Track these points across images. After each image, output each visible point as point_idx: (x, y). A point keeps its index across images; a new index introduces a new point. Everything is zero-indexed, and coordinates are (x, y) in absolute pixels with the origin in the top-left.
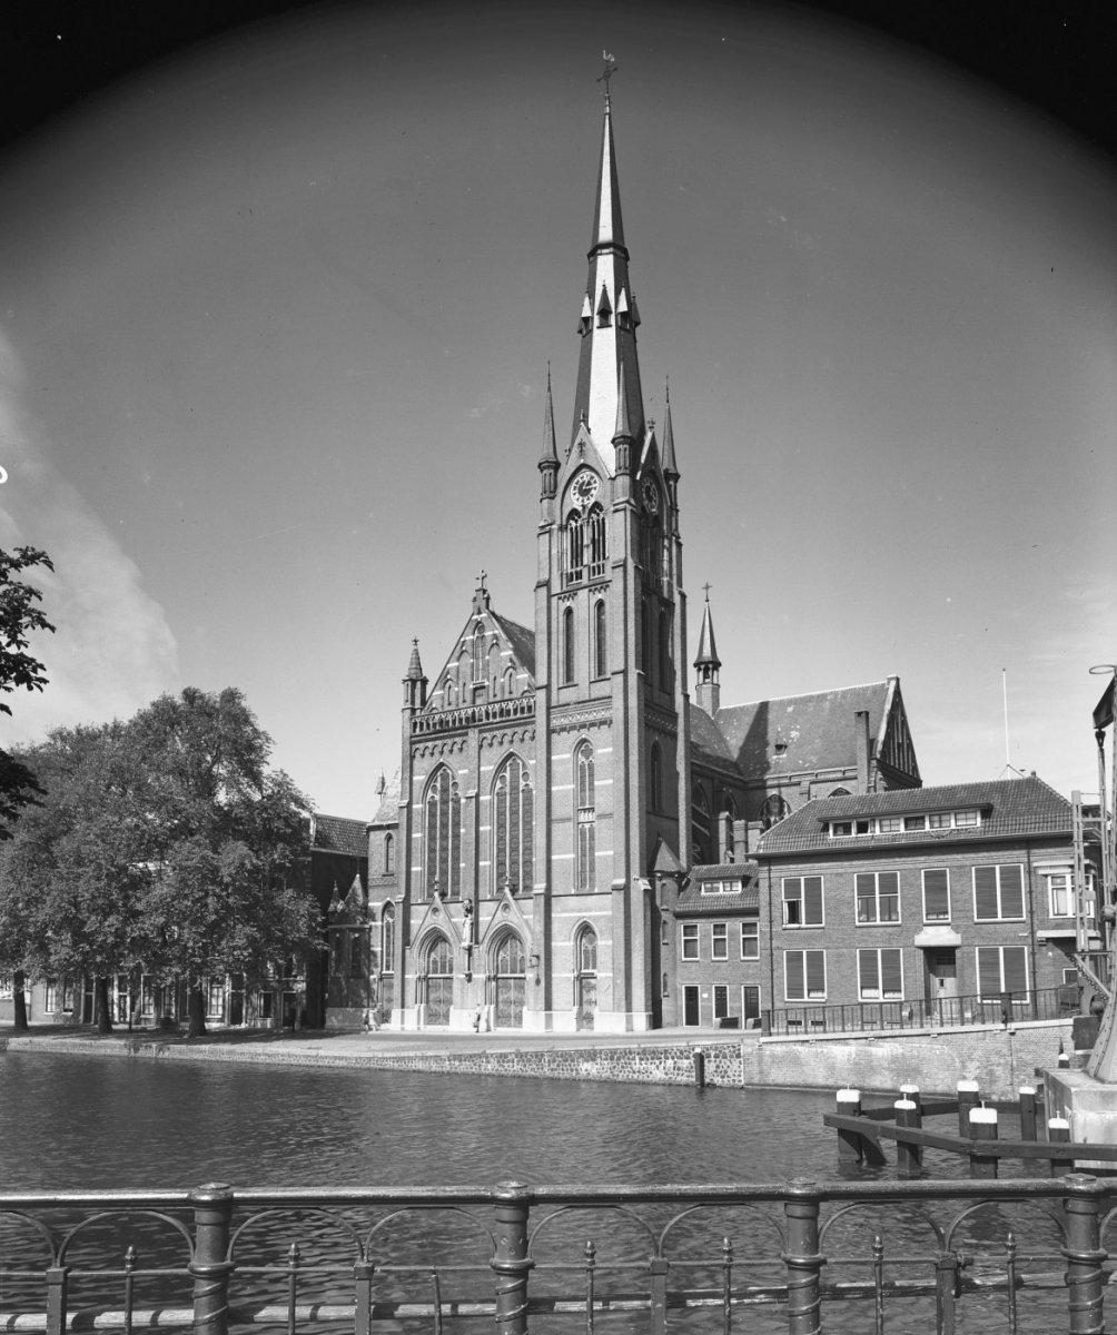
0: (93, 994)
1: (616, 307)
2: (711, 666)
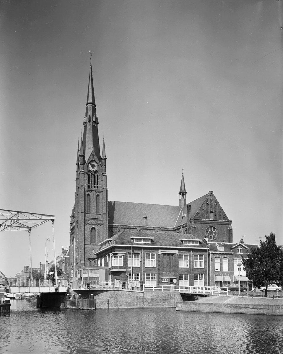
0: (163, 285)
1: (93, 120)
2: (184, 194)
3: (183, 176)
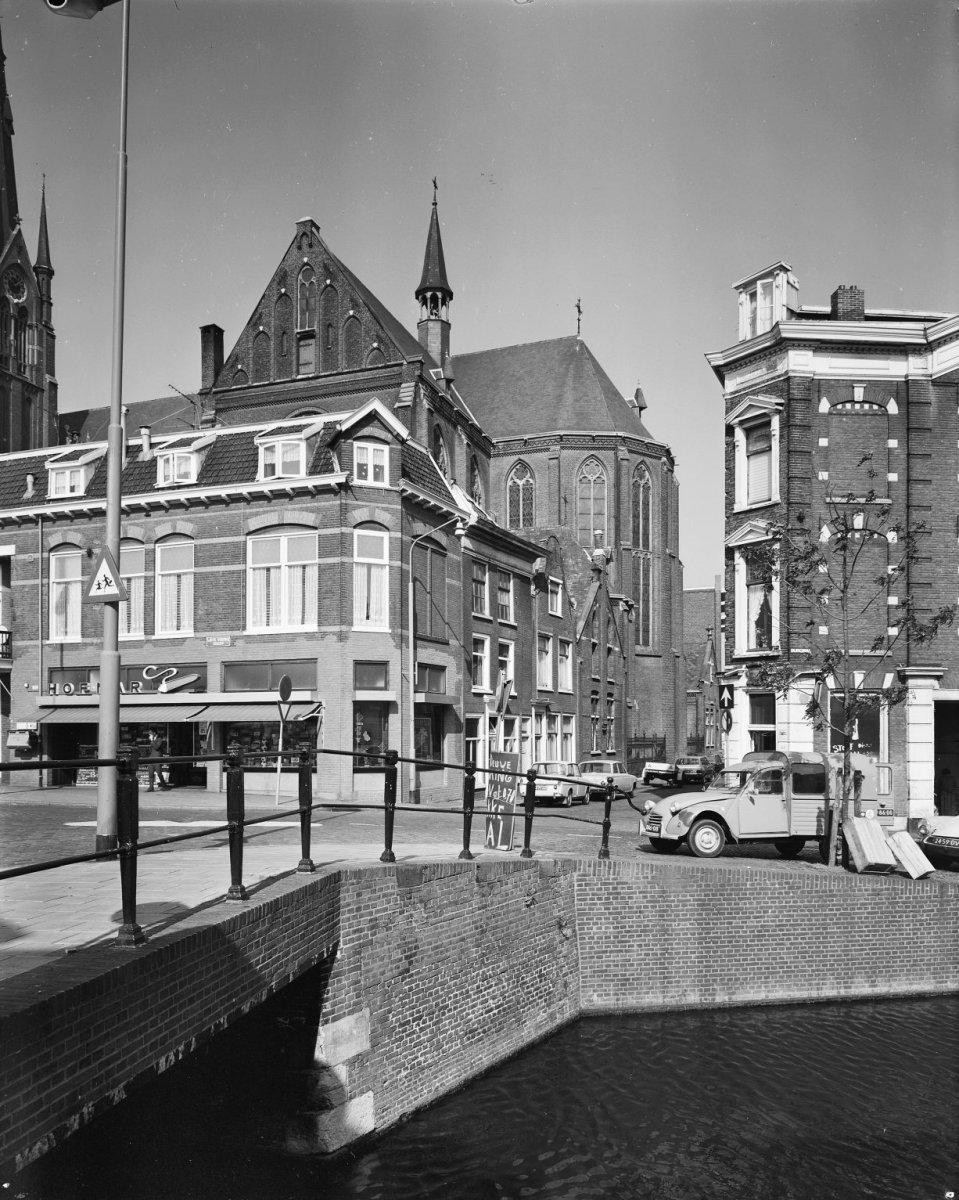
3: (435, 212)
